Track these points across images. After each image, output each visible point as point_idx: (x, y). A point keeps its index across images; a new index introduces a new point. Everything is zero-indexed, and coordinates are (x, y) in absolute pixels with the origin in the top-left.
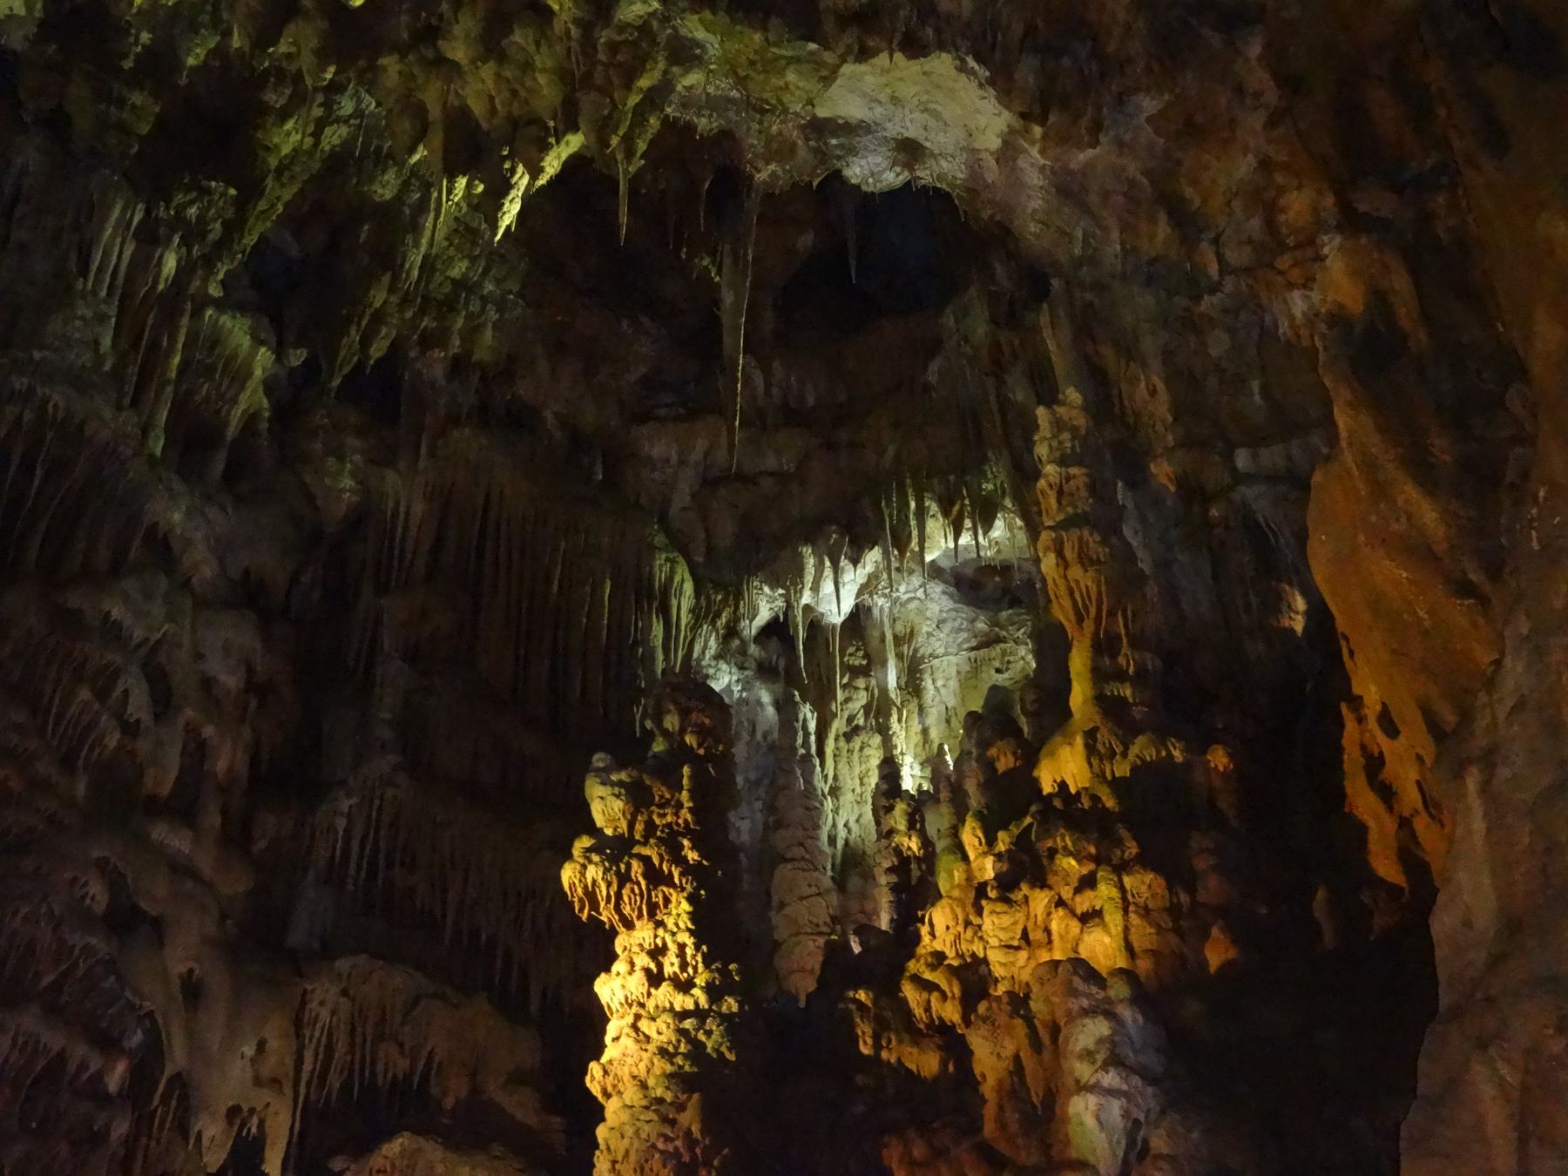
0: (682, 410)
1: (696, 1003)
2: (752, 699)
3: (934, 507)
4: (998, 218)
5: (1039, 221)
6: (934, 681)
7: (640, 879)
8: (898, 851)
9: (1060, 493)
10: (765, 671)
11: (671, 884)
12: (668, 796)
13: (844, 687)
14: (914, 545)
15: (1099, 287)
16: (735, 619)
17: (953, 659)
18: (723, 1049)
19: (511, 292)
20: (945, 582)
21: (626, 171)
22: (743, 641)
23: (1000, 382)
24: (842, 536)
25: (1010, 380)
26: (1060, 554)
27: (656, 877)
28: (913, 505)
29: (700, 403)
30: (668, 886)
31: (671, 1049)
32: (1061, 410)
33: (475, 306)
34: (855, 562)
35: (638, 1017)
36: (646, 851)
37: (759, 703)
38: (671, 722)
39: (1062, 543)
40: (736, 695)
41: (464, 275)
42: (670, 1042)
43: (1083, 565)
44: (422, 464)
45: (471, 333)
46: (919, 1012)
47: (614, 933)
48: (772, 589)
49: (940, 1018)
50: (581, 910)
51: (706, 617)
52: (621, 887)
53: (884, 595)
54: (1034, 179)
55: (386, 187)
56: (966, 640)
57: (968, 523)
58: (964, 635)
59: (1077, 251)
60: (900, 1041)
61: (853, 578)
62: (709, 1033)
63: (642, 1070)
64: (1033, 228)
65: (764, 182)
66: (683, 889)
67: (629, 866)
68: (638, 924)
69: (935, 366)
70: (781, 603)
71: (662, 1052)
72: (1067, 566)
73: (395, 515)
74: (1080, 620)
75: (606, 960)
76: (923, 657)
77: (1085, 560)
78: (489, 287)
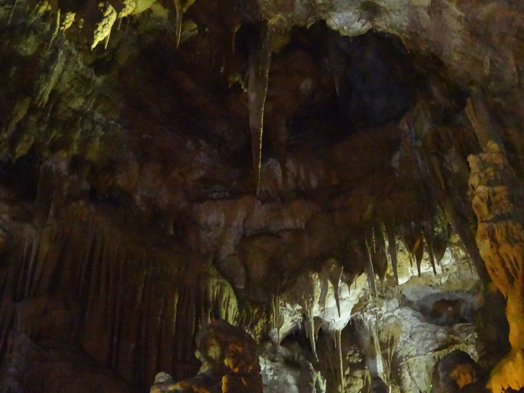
0: (227, 194)
2: (281, 381)
3: (401, 245)
4: (432, 50)
5: (459, 52)
6: (410, 373)
9: (489, 204)
10: (290, 363)
13: (347, 377)
14: (389, 271)
15: (505, 94)
16: (268, 327)
17: (423, 358)
19: (112, 119)
20: (413, 309)
21: (181, 10)
22: (273, 344)
23: (442, 160)
24: (340, 266)
25: (448, 158)
26: (493, 239)
28: (387, 243)
29: (241, 187)
32: (484, 156)
33: (88, 126)
34: (349, 283)
37: (286, 383)
38: (214, 352)
39: (493, 231)
40: (270, 378)
41: (81, 107)
43: (510, 243)
44: (50, 221)
45: (86, 141)
48: (292, 305)
51: (247, 324)
53: (372, 313)
54: (455, 26)
55: (28, 47)
56: (432, 345)
57: (426, 255)
58: (429, 342)
59: (486, 72)
61: (350, 295)
64: (456, 57)
65: (274, 25)
69: (397, 157)
70: (299, 317)
72: (498, 246)
73: (30, 248)
74: (511, 280)
76: (402, 357)
77: (510, 239)
78: (98, 116)
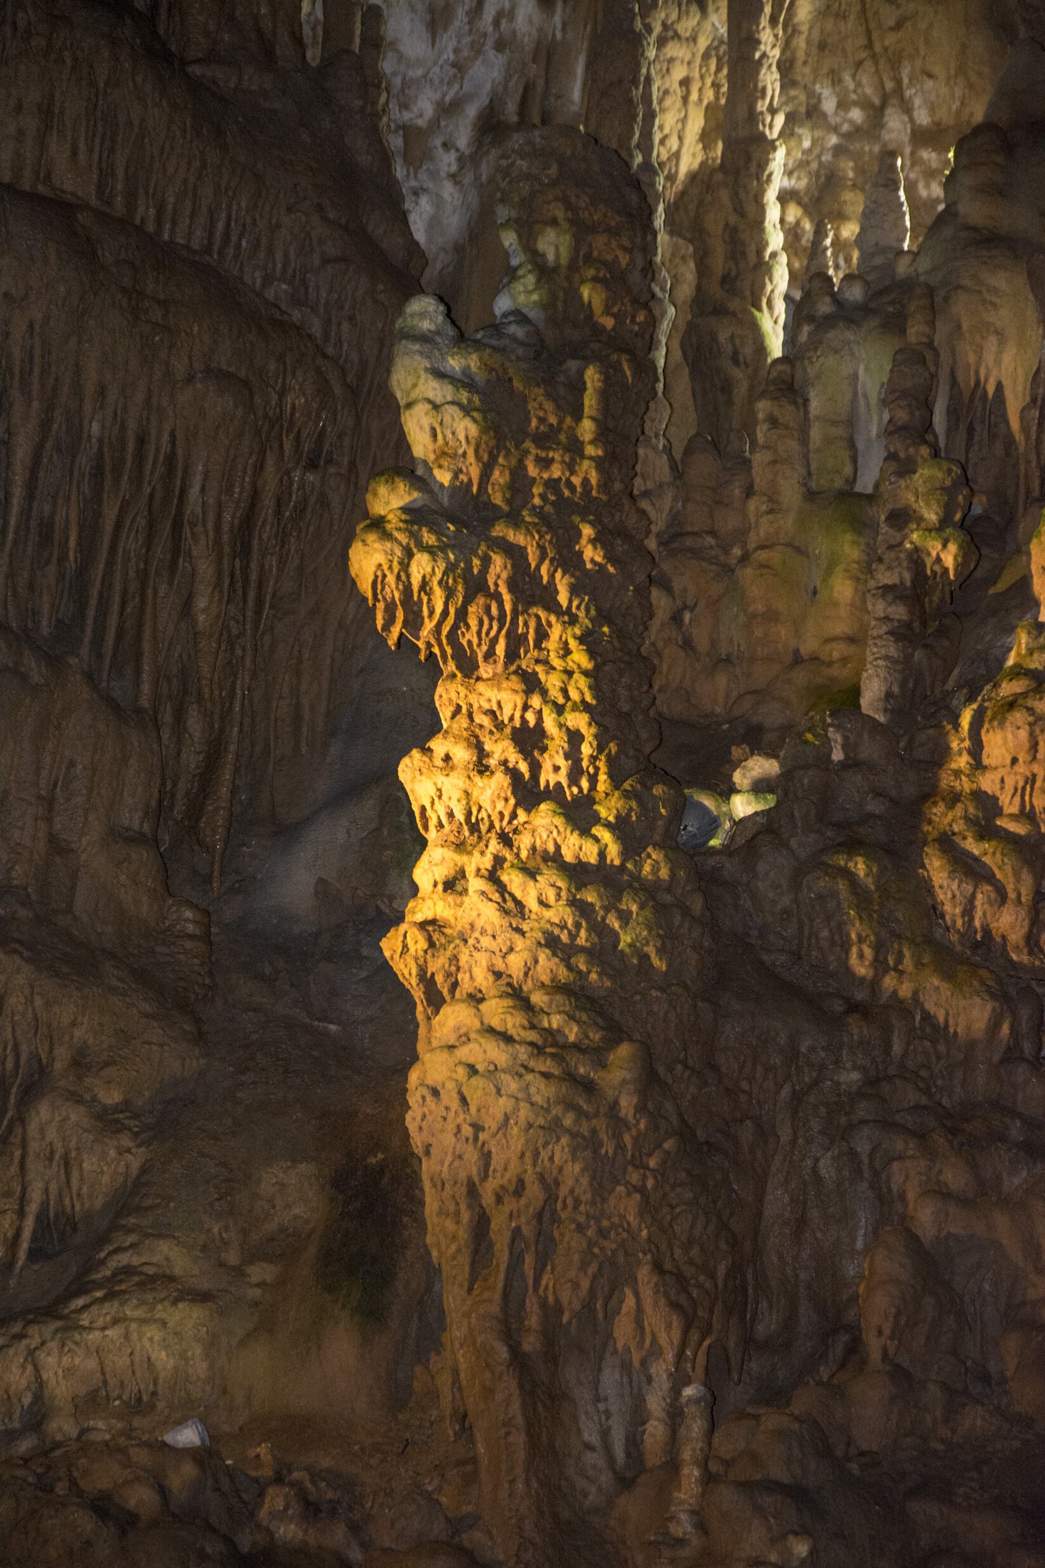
1: (602, 855)
7: (503, 589)
8: (916, 559)
11: (552, 606)
12: (553, 420)
18: (651, 950)
27: (530, 592)
30: (548, 609)
31: (564, 937)
35: (499, 861)
36: (517, 537)
38: (554, 244)
42: (563, 926)
46: (952, 911)
47: (432, 670)
49: (987, 931)
50: (387, 627)
52: (468, 600)
60: (919, 964)
62: (625, 917)
63: (516, 963)
66: (573, 620)
67: (486, 561)
68: (485, 670)
71: (551, 942)
75: (423, 728)
